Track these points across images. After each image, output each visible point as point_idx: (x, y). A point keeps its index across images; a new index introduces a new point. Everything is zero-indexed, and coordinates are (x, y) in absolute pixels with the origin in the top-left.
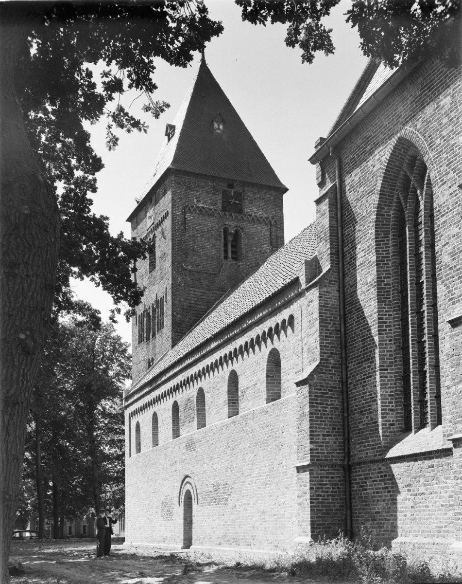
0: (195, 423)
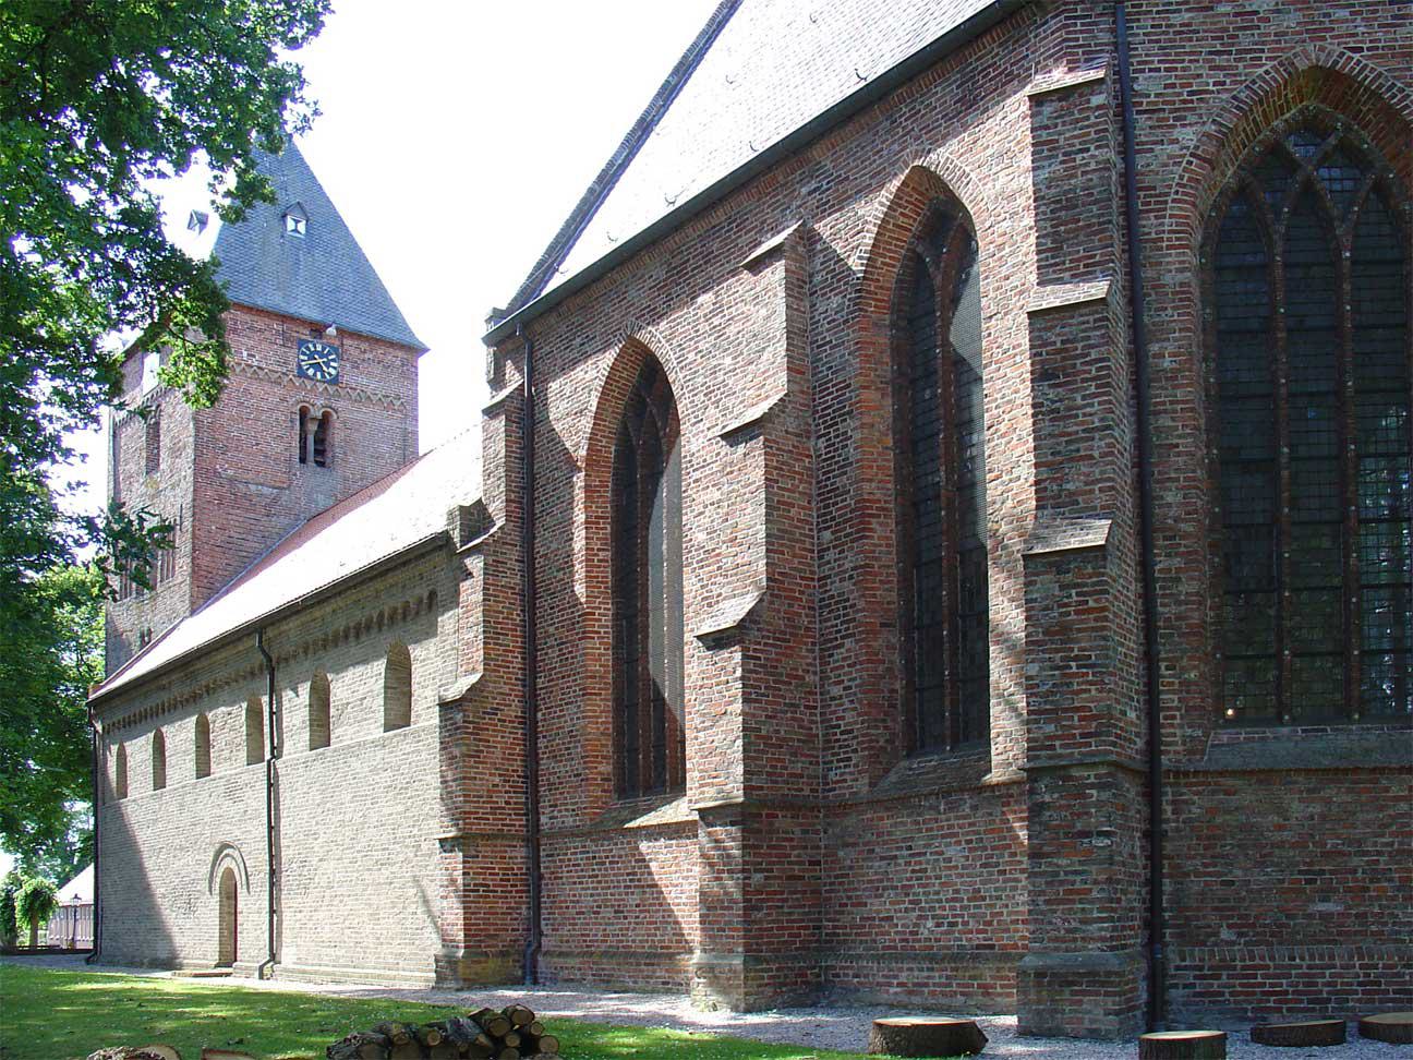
0: (243, 754)
